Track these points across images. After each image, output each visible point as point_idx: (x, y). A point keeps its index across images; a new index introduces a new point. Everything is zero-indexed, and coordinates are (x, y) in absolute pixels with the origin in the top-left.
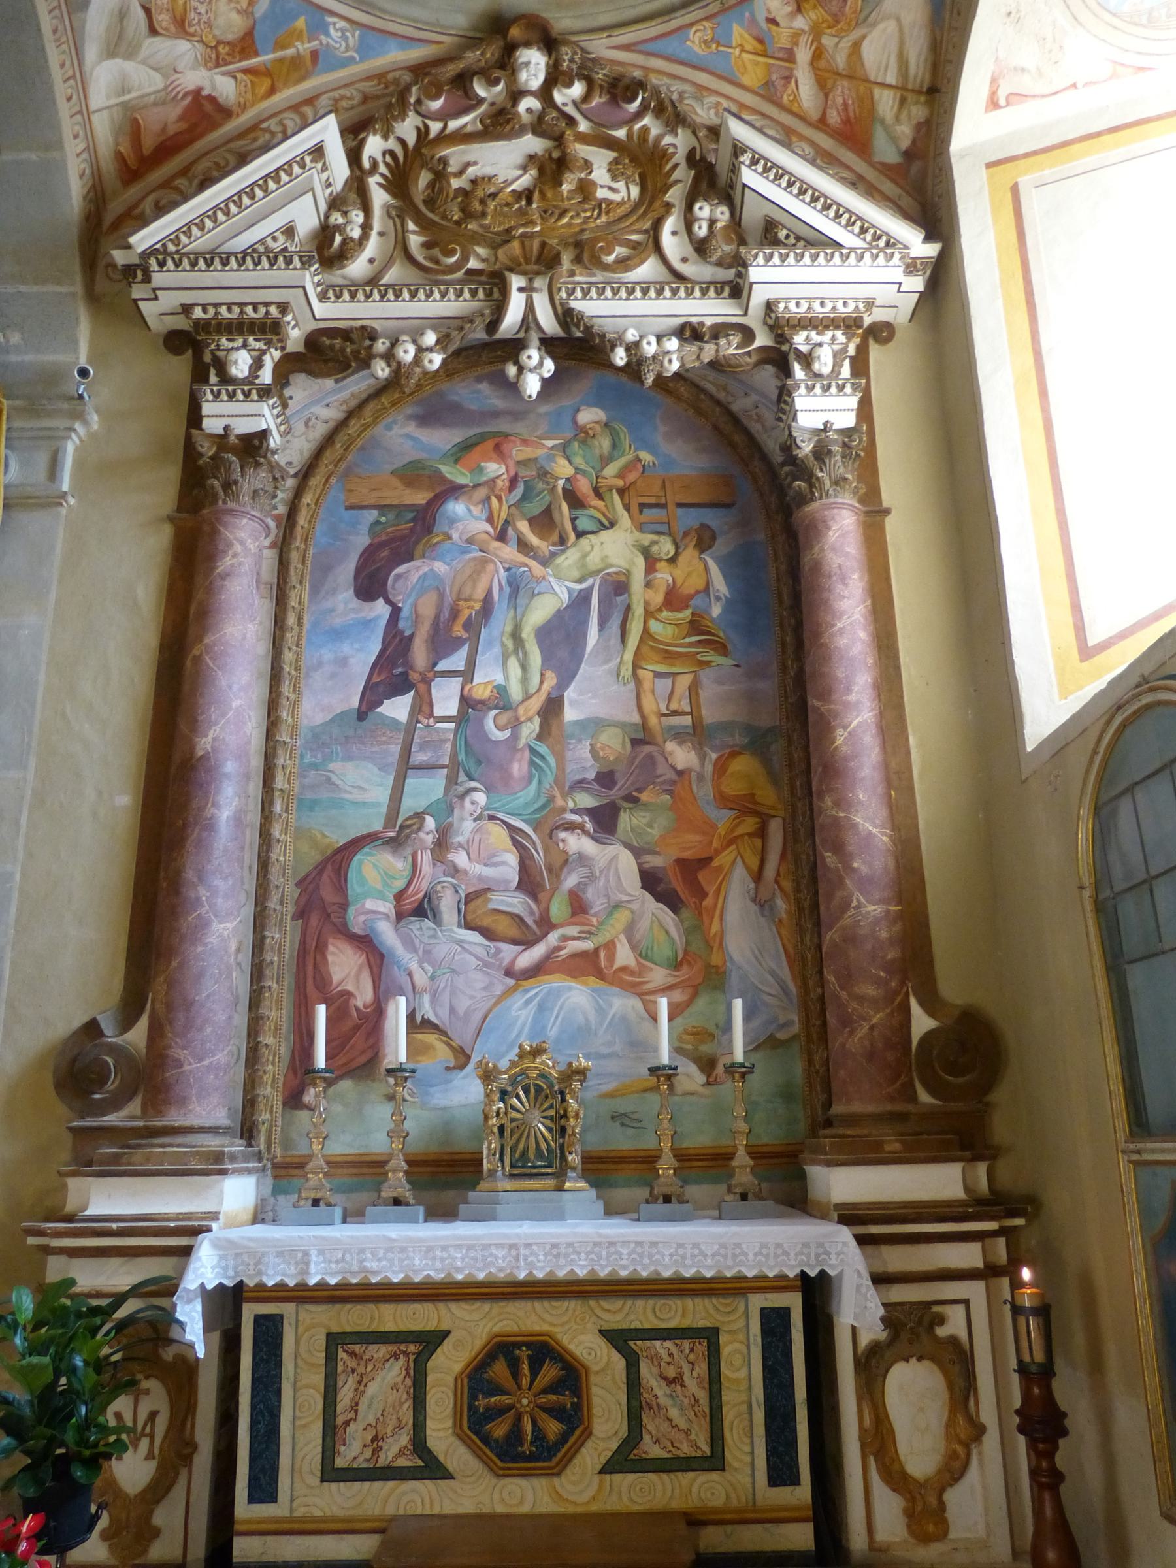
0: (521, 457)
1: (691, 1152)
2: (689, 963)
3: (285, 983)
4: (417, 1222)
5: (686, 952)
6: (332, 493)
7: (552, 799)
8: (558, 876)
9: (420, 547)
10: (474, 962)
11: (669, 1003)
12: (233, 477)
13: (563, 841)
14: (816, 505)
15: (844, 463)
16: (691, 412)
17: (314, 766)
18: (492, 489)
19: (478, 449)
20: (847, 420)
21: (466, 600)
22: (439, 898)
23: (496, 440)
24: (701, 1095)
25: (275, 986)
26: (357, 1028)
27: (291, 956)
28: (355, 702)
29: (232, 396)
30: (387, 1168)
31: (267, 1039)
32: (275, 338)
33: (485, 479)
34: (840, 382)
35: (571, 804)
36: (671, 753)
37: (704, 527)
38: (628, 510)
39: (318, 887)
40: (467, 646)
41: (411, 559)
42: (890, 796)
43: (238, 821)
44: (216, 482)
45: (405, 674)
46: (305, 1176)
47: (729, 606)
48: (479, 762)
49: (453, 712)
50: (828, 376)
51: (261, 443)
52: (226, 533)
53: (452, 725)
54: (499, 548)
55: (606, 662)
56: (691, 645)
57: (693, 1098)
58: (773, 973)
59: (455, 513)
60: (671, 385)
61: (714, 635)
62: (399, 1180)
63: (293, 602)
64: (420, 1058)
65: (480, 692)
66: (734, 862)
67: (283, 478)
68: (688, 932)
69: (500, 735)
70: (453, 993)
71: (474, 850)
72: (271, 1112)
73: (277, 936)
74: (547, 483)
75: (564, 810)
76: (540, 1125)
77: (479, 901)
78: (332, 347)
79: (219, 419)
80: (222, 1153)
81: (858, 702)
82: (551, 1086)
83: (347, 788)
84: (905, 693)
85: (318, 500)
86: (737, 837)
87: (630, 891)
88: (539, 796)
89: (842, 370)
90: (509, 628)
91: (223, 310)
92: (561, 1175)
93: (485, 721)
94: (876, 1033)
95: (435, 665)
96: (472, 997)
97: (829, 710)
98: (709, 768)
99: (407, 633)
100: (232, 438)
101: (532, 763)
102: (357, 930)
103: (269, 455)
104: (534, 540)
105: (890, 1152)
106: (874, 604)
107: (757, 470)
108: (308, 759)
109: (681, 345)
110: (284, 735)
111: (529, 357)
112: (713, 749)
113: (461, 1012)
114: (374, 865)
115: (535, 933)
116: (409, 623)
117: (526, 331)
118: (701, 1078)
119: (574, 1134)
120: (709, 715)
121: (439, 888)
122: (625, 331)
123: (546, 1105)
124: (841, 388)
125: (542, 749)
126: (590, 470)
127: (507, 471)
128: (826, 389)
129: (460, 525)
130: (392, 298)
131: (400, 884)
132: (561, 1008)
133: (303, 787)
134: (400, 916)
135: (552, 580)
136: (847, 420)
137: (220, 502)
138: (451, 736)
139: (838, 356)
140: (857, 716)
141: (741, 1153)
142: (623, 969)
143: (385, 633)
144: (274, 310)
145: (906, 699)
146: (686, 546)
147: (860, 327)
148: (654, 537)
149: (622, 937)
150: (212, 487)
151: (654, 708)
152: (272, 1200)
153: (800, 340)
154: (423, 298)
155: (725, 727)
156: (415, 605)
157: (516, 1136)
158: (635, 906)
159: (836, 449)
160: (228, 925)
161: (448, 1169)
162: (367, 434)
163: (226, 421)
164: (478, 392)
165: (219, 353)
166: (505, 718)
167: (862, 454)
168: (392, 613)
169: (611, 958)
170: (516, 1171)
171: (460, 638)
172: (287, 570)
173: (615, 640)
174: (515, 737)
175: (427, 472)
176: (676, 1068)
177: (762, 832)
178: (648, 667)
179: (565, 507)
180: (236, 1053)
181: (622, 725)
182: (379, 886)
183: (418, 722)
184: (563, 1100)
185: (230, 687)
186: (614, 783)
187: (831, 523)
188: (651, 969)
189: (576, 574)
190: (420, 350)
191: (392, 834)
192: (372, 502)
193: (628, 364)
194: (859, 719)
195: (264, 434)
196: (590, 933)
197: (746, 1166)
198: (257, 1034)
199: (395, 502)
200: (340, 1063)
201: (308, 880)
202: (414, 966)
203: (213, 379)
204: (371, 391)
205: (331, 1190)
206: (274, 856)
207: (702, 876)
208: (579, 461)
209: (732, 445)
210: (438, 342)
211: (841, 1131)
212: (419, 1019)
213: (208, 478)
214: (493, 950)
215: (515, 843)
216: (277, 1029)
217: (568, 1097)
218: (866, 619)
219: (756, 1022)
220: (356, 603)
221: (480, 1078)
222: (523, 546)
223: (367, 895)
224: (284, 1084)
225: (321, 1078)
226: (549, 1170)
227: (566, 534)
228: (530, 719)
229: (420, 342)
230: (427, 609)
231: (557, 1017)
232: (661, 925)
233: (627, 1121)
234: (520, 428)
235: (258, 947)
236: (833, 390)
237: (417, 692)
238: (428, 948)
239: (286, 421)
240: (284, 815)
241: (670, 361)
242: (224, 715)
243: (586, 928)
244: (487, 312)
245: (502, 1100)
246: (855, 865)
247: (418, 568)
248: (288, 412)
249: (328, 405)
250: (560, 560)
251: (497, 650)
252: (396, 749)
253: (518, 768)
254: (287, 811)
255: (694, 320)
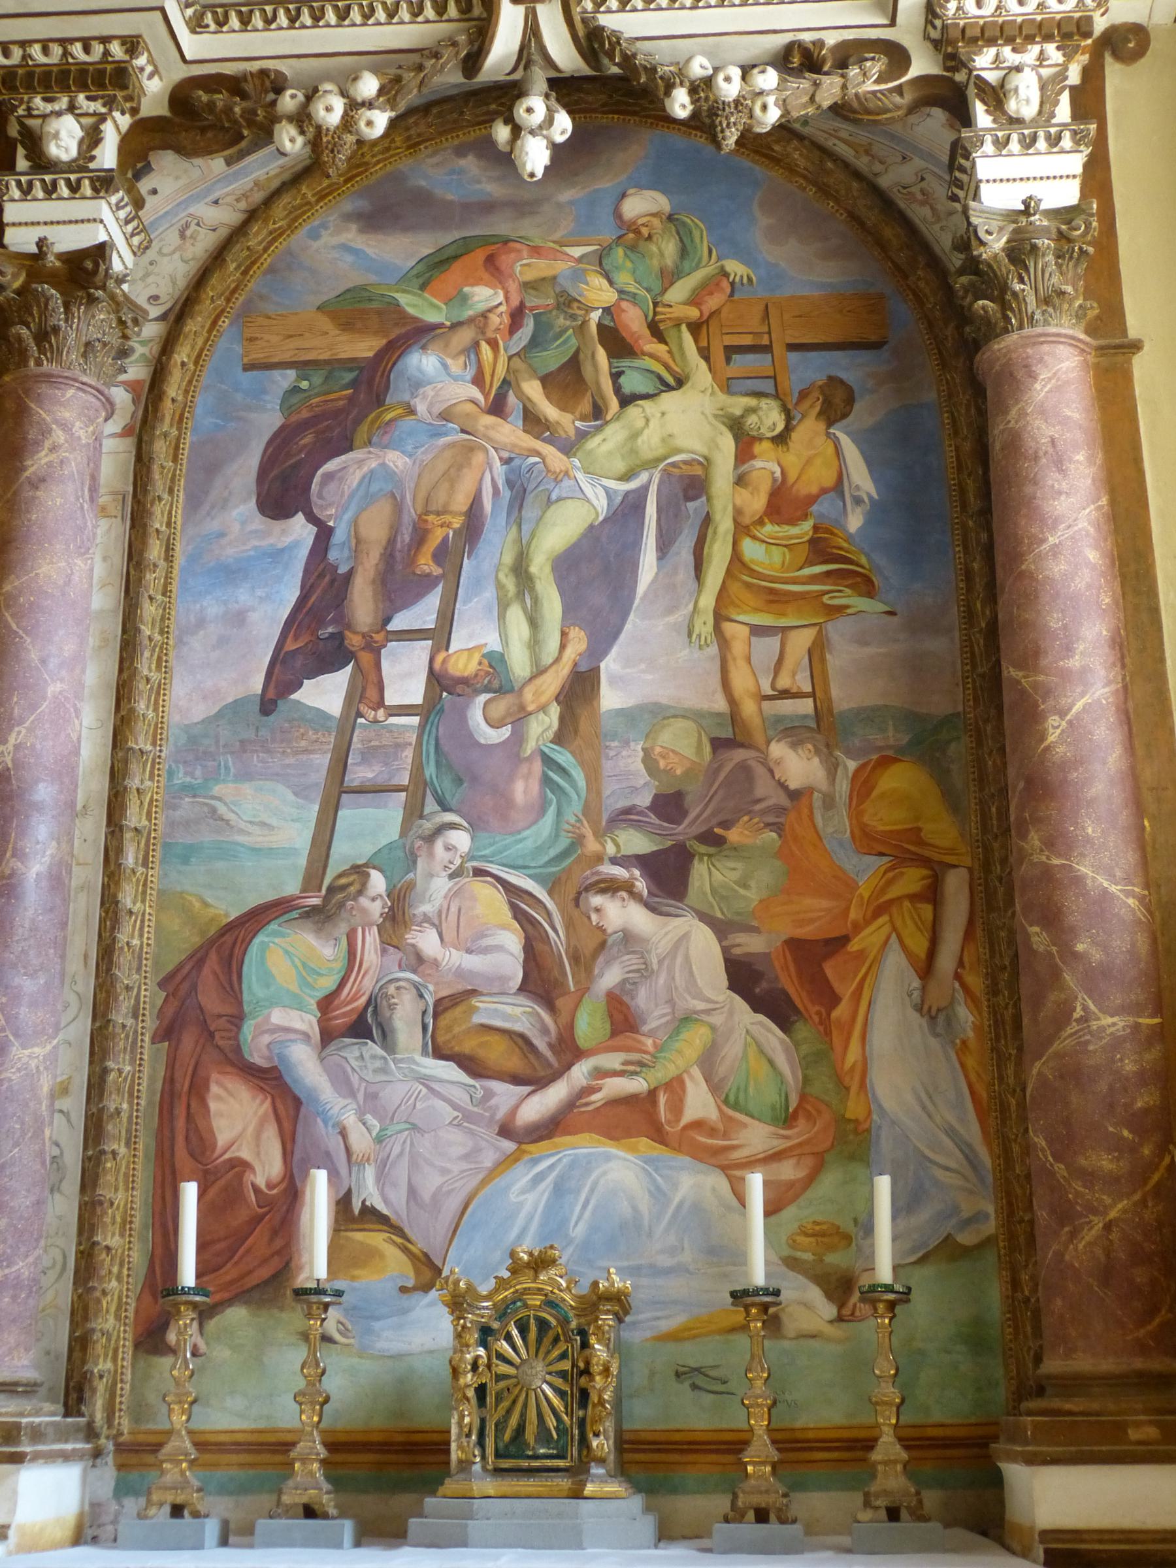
0: (530, 276)
1: (811, 1435)
2: (809, 1117)
3: (140, 1146)
4: (338, 1545)
5: (803, 1097)
6: (222, 344)
7: (579, 841)
8: (589, 970)
9: (364, 429)
10: (449, 1113)
11: (766, 1184)
12: (53, 321)
13: (597, 910)
14: (1013, 338)
15: (1059, 266)
16: (811, 191)
17: (189, 790)
18: (482, 331)
19: (457, 266)
20: (1067, 194)
21: (438, 514)
22: (392, 1007)
23: (490, 250)
24: (828, 1339)
25: (123, 1150)
26: (257, 1220)
27: (150, 1103)
28: (257, 684)
29: (50, 191)
30: (292, 1455)
31: (110, 1238)
32: (120, 95)
33: (471, 313)
34: (1053, 130)
35: (611, 849)
36: (778, 762)
37: (834, 381)
38: (707, 359)
39: (194, 988)
40: (439, 589)
41: (350, 449)
42: (1143, 827)
43: (57, 880)
44: (24, 331)
45: (339, 637)
46: (158, 1465)
47: (878, 513)
48: (459, 781)
49: (418, 699)
50: (1033, 120)
51: (97, 265)
52: (41, 413)
53: (415, 720)
54: (493, 427)
55: (671, 610)
56: (813, 579)
57: (814, 1344)
58: (951, 1132)
59: (420, 370)
60: (777, 148)
61: (851, 562)
62: (312, 1474)
63: (158, 522)
64: (357, 1272)
65: (461, 665)
66: (888, 938)
67: (136, 322)
68: (809, 1063)
69: (493, 736)
70: (414, 1164)
71: (449, 927)
72: (115, 1359)
73: (128, 1068)
74: (573, 317)
75: (599, 859)
76: (545, 1387)
77: (458, 1011)
78: (211, 105)
79: (31, 228)
80: (17, 1426)
81: (1085, 670)
82: (563, 1322)
83: (242, 825)
84: (1168, 654)
85: (199, 356)
86: (891, 902)
87: (709, 993)
88: (557, 836)
89: (1058, 110)
90: (508, 559)
91: (36, 51)
92: (579, 1472)
93: (469, 714)
94: (1114, 1236)
95: (387, 620)
96: (444, 1171)
97: (1036, 686)
98: (843, 786)
99: (342, 570)
100: (51, 258)
101: (546, 781)
102: (258, 1060)
103: (111, 284)
104: (550, 411)
105: (1140, 1443)
106: (1113, 502)
107: (922, 284)
108: (181, 778)
109: (782, 81)
110: (141, 739)
111: (529, 110)
112: (849, 753)
113: (426, 1195)
114: (287, 952)
115: (550, 1065)
116: (346, 553)
117: (526, 68)
118: (828, 1310)
119: (601, 1402)
120: (843, 697)
121: (391, 989)
122: (688, 60)
123: (556, 1353)
124: (1054, 141)
125: (564, 757)
126: (643, 293)
127: (507, 298)
128: (1028, 143)
129: (429, 390)
130: (309, 22)
131: (328, 984)
132: (592, 1190)
133: (172, 824)
134: (328, 1036)
135: (580, 476)
136: (1067, 194)
137: (32, 363)
138: (413, 738)
139: (1048, 90)
140: (1083, 694)
141: (887, 1438)
142: (698, 1125)
143: (306, 571)
144: (116, 49)
145: (1169, 662)
146: (803, 416)
147: (1087, 34)
148: (752, 402)
149: (696, 1072)
150: (20, 339)
151: (750, 684)
152: (114, 1507)
153: (984, 61)
154: (358, 20)
155: (869, 716)
156: (355, 522)
157: (505, 1404)
158: (717, 1019)
159: (1044, 243)
160: (36, 1050)
161: (402, 1458)
162: (281, 245)
163: (40, 232)
164: (461, 172)
165: (31, 122)
166: (501, 707)
167: (1091, 250)
168: (317, 537)
169: (677, 1107)
170: (506, 1464)
171: (428, 575)
172: (149, 470)
173: (685, 572)
174: (518, 738)
175: (374, 305)
176: (777, 1293)
177: (933, 894)
178: (741, 618)
179: (601, 355)
180: (59, 1259)
181: (696, 716)
182: (294, 987)
183: (360, 715)
184: (585, 1345)
185: (43, 661)
186: (684, 813)
187: (1037, 369)
188: (745, 1126)
189: (620, 466)
190: (353, 105)
191: (315, 901)
192: (287, 357)
193: (695, 115)
194: (1086, 699)
195: (101, 251)
196: (641, 1064)
197: (895, 1462)
198: (92, 1230)
199: (325, 356)
200: (228, 1278)
201: (179, 977)
202: (350, 1119)
203: (22, 164)
204: (286, 176)
205: (200, 1490)
206: (122, 938)
207: (829, 969)
208: (624, 279)
209: (881, 244)
210: (381, 91)
211: (1056, 1403)
212: (357, 1206)
213: (14, 324)
214: (480, 1094)
215: (519, 914)
216: (126, 1222)
217: (593, 1340)
218: (1098, 529)
219: (924, 1215)
220: (259, 522)
221: (447, 1305)
222: (533, 422)
223: (272, 1003)
224: (137, 1312)
225: (187, 1303)
226: (561, 1463)
227: (603, 398)
228: (543, 708)
229: (352, 92)
230: (375, 530)
231: (585, 1206)
232: (762, 1052)
233: (700, 1381)
234: (529, 229)
235: (97, 1086)
236: (1041, 144)
237: (358, 668)
238: (372, 1089)
239: (142, 229)
240: (141, 870)
241: (764, 107)
242: (33, 707)
243: (635, 1056)
244: (462, 38)
245: (484, 1343)
246: (1080, 947)
247: (361, 462)
248: (146, 214)
249: (216, 202)
250: (593, 443)
251: (489, 594)
252: (322, 760)
253: (524, 790)
254: (145, 864)
255: (807, 37)
